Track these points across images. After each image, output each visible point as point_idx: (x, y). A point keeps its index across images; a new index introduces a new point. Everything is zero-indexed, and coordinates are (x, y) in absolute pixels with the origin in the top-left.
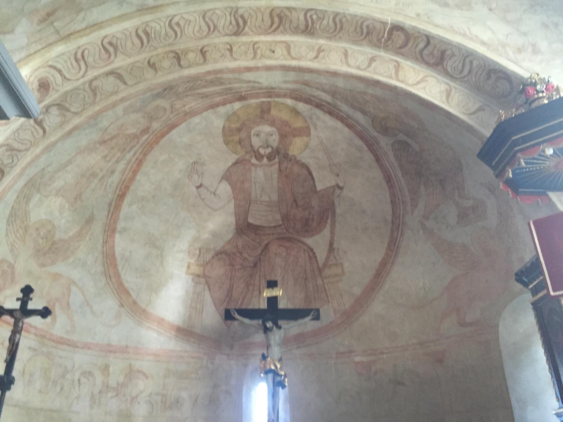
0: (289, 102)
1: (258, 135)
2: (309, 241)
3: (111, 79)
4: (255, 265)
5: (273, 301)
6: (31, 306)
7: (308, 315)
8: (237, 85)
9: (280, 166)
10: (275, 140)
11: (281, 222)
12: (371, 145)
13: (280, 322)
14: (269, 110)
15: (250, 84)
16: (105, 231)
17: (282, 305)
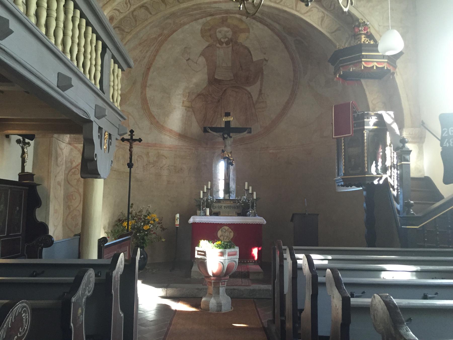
0: (238, 16)
1: (220, 32)
2: (248, 89)
3: (143, 10)
4: (219, 101)
5: (228, 123)
6: (134, 137)
7: (245, 131)
8: (209, 10)
9: (232, 48)
10: (230, 35)
11: (233, 78)
12: (283, 40)
13: (231, 134)
14: (227, 20)
15: (215, 9)
16: (141, 87)
17: (232, 125)
